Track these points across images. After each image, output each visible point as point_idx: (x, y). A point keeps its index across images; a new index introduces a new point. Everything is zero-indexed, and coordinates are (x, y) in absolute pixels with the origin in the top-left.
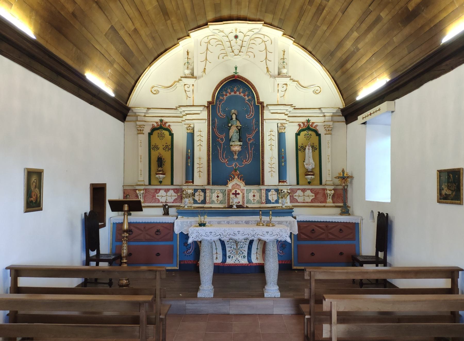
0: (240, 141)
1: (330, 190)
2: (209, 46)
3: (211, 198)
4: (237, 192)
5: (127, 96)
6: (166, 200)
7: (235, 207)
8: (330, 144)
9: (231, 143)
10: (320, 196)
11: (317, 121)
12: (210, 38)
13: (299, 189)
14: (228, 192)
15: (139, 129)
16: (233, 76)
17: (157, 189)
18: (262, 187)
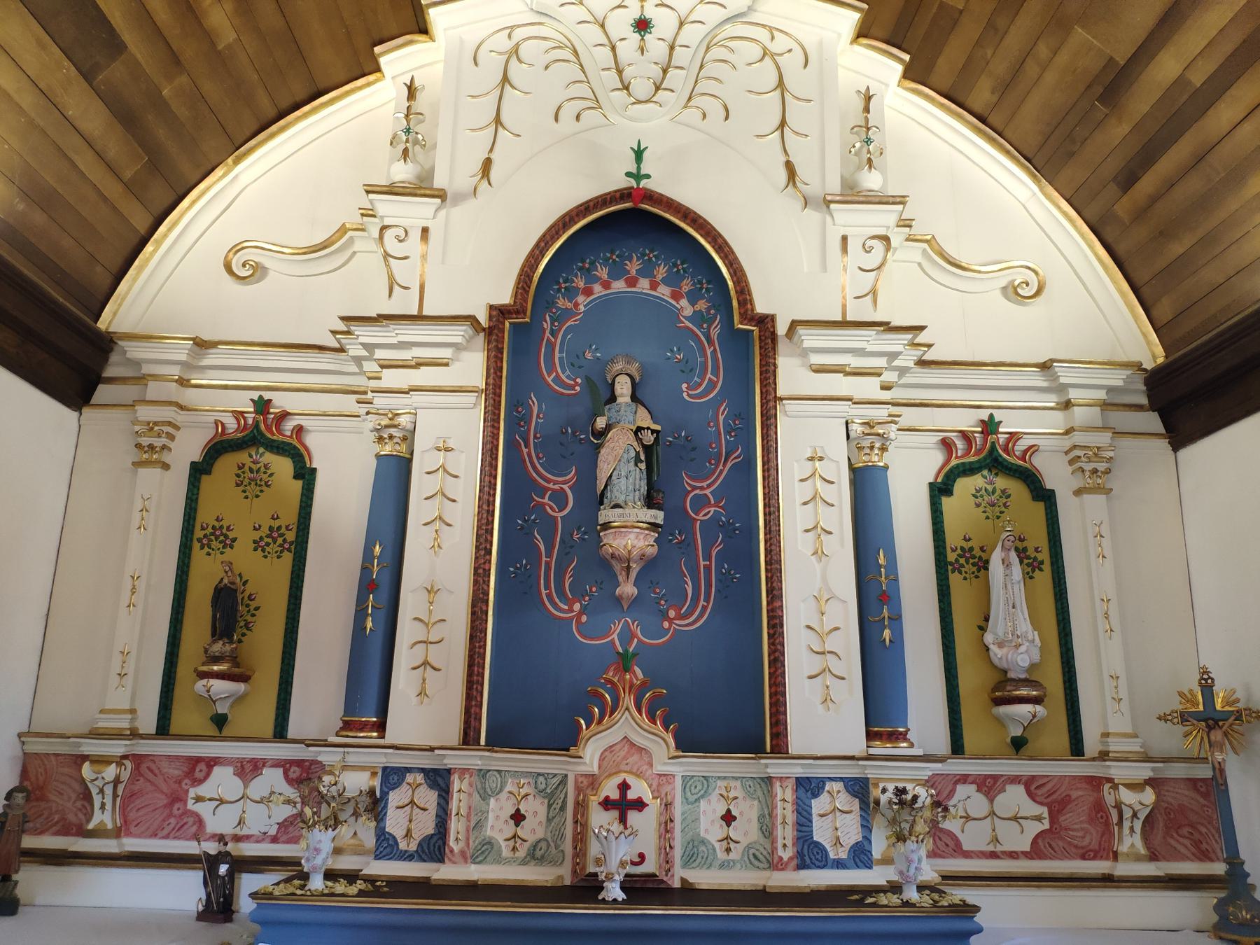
0: (650, 502)
1: (1134, 787)
2: (515, 70)
3: (479, 825)
4: (631, 795)
5: (108, 281)
6: (241, 822)
7: (614, 891)
8: (1106, 543)
9: (605, 515)
10: (1075, 818)
11: (1031, 423)
12: (519, 34)
13: (964, 779)
14: (578, 790)
15: (145, 441)
16: (624, 194)
18: (774, 767)
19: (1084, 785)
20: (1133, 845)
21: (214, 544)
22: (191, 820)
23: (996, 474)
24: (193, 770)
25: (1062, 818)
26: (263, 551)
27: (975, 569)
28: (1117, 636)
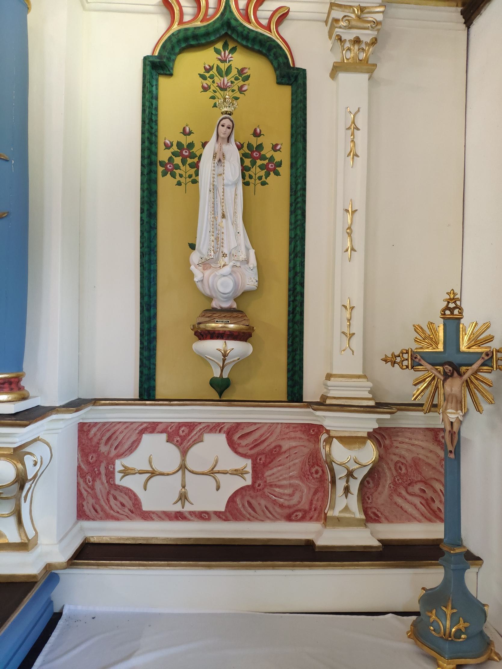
1: (349, 441)
6: (183, 497)
8: (361, 137)
10: (285, 474)
13: (152, 428)
19: (299, 434)
20: (346, 509)
23: (233, 50)
25: (268, 473)
27: (263, 173)
28: (359, 256)
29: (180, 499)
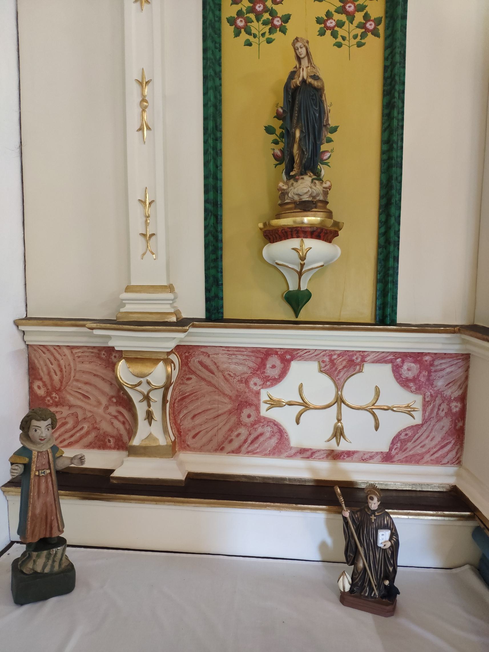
6: (338, 433)
17: (268, 353)
20: (150, 436)
21: (256, 27)
22: (268, 430)
24: (262, 365)
26: (334, 35)
29: (335, 435)
